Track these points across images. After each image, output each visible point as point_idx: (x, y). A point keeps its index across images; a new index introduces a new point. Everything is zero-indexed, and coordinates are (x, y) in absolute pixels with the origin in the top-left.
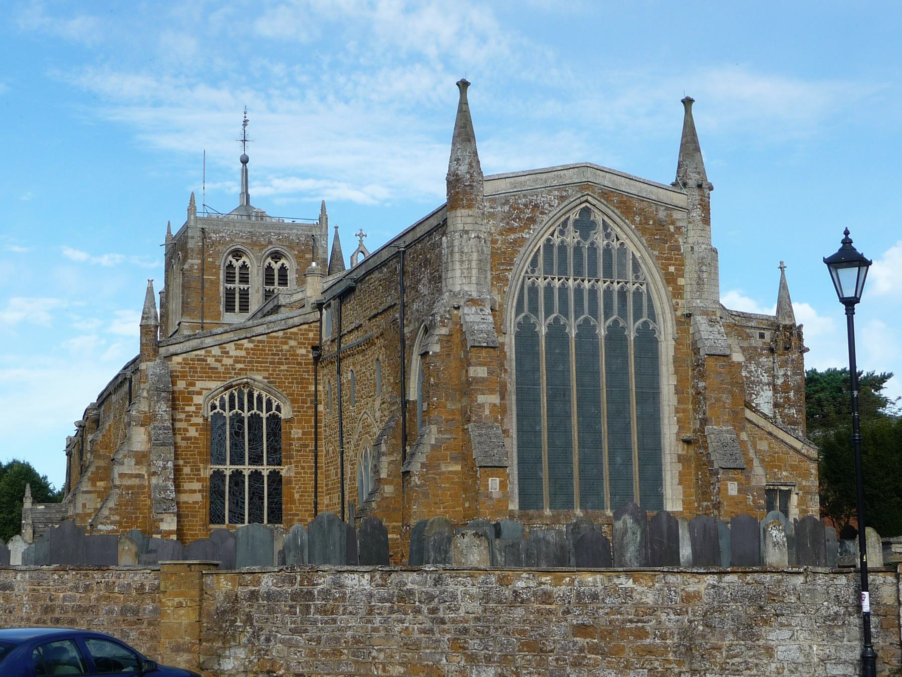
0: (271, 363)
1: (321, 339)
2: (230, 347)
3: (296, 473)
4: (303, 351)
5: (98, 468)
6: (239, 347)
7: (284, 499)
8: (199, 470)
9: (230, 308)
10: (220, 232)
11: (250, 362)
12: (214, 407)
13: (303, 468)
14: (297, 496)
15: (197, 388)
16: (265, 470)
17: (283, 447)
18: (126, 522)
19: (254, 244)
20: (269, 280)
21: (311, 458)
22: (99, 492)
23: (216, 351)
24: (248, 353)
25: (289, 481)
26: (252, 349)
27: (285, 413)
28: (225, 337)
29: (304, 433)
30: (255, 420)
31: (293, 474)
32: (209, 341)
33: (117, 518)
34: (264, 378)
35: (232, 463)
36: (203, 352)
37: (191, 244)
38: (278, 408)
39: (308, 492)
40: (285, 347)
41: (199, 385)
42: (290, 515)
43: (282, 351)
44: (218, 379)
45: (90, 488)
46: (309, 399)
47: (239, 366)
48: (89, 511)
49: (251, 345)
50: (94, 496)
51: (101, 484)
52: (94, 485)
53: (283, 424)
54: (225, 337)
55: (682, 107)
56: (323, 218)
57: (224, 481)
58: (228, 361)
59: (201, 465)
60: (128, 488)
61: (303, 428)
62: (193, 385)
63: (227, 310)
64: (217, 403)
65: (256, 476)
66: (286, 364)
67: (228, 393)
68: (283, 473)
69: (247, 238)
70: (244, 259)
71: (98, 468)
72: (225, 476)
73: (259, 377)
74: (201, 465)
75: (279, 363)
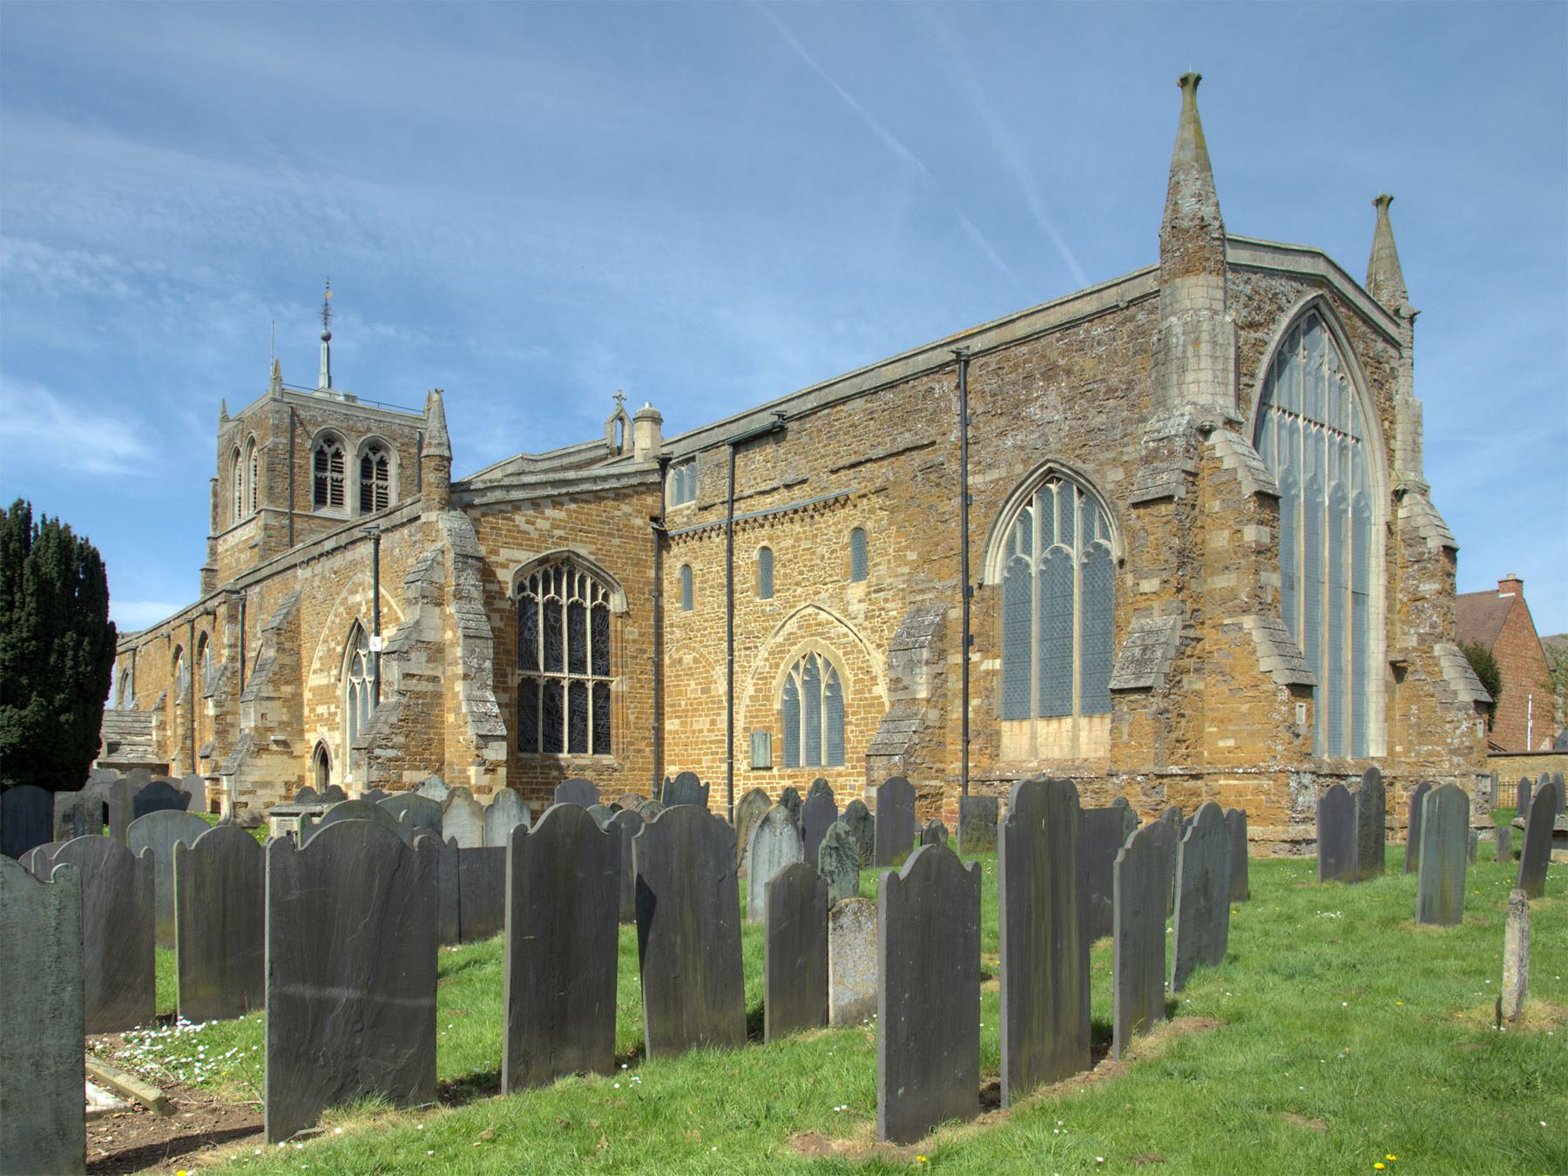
0: (601, 533)
4: (639, 522)
5: (282, 666)
7: (613, 721)
8: (505, 676)
11: (572, 529)
13: (640, 681)
15: (501, 559)
17: (612, 650)
22: (286, 700)
29: (642, 635)
33: (401, 739)
35: (561, 670)
38: (606, 597)
40: (617, 513)
41: (505, 554)
44: (531, 548)
47: (558, 532)
52: (277, 688)
53: (612, 619)
55: (1372, 213)
57: (536, 695)
58: (543, 524)
59: (509, 670)
62: (496, 553)
64: (527, 583)
67: (541, 569)
72: (537, 686)
73: (583, 552)
74: (509, 670)
75: (612, 535)
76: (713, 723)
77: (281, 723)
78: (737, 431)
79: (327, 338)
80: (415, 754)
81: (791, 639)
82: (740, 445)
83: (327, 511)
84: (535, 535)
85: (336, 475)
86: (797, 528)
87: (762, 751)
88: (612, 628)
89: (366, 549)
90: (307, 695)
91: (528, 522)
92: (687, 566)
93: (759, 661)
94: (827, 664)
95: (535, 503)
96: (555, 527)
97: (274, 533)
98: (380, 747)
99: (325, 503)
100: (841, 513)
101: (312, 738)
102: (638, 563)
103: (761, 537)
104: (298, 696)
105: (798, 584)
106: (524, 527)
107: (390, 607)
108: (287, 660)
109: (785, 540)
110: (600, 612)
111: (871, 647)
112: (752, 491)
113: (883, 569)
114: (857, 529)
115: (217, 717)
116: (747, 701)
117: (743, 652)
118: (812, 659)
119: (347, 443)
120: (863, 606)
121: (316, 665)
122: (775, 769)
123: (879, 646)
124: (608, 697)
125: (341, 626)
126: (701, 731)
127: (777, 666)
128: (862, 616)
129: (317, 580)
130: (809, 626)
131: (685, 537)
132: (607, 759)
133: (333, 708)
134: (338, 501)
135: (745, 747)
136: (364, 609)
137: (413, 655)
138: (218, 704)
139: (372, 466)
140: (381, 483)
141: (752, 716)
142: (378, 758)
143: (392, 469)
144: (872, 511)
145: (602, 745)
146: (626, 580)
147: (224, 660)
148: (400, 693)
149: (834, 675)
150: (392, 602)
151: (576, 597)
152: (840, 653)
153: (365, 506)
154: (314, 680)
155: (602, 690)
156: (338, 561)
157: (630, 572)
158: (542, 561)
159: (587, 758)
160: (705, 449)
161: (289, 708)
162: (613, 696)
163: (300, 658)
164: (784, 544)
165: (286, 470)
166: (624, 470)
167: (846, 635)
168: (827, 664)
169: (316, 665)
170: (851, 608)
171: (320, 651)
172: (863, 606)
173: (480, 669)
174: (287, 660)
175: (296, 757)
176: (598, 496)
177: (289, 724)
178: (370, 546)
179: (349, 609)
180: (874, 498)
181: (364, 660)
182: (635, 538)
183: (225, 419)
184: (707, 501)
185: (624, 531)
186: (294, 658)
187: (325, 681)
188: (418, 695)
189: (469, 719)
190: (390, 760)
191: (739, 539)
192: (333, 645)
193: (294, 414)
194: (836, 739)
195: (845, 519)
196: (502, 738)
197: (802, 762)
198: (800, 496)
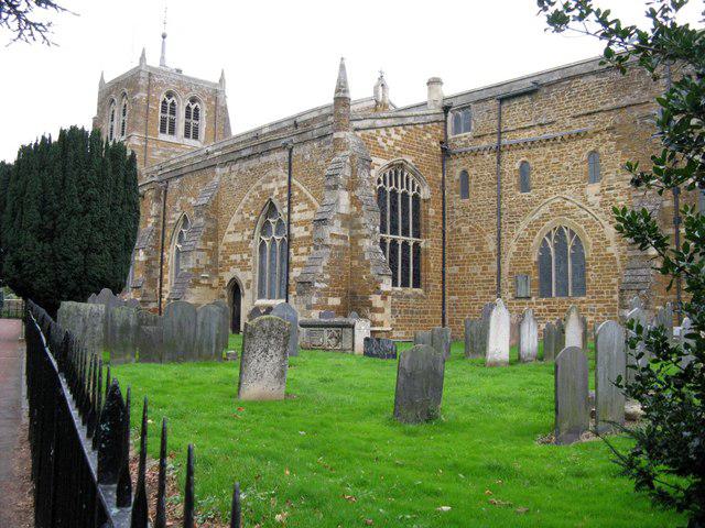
1: (447, 136)
2: (392, 131)
6: (397, 132)
9: (163, 130)
12: (379, 182)
14: (432, 265)
16: (411, 240)
20: (188, 115)
21: (440, 234)
23: (383, 132)
27: (425, 193)
28: (390, 122)
30: (405, 195)
32: (379, 123)
33: (328, 276)
36: (374, 131)
37: (142, 82)
38: (418, 190)
44: (384, 157)
47: (398, 148)
49: (404, 132)
51: (210, 243)
54: (390, 122)
56: (222, 80)
60: (337, 248)
63: (161, 132)
65: (405, 244)
68: (422, 245)
70: (173, 98)
73: (409, 161)
76: (485, 269)
77: (207, 266)
78: (501, 92)
81: (545, 218)
82: (502, 100)
84: (386, 149)
86: (548, 150)
87: (523, 287)
89: (282, 156)
90: (222, 248)
92: (465, 172)
93: (521, 230)
94: (572, 233)
96: (396, 144)
99: (165, 132)
100: (580, 143)
103: (522, 155)
105: (548, 184)
107: (301, 192)
109: (538, 158)
110: (416, 198)
111: (605, 223)
112: (514, 128)
113: (612, 176)
114: (594, 152)
116: (512, 256)
117: (508, 225)
118: (560, 230)
120: (599, 198)
122: (533, 299)
123: (611, 223)
126: (476, 274)
127: (534, 234)
128: (598, 204)
129: (233, 176)
130: (558, 210)
131: (464, 154)
135: (509, 284)
136: (276, 193)
138: (147, 254)
139: (193, 114)
141: (514, 264)
143: (203, 114)
144: (604, 141)
149: (577, 239)
151: (405, 189)
152: (582, 226)
153: (187, 135)
158: (391, 166)
160: (476, 102)
164: (538, 160)
166: (418, 113)
167: (586, 216)
168: (572, 233)
169: (231, 228)
170: (589, 200)
171: (236, 218)
172: (599, 198)
178: (285, 154)
180: (605, 134)
184: (479, 133)
187: (240, 239)
191: (505, 155)
194: (578, 280)
195: (584, 146)
197: (554, 294)
198: (549, 132)
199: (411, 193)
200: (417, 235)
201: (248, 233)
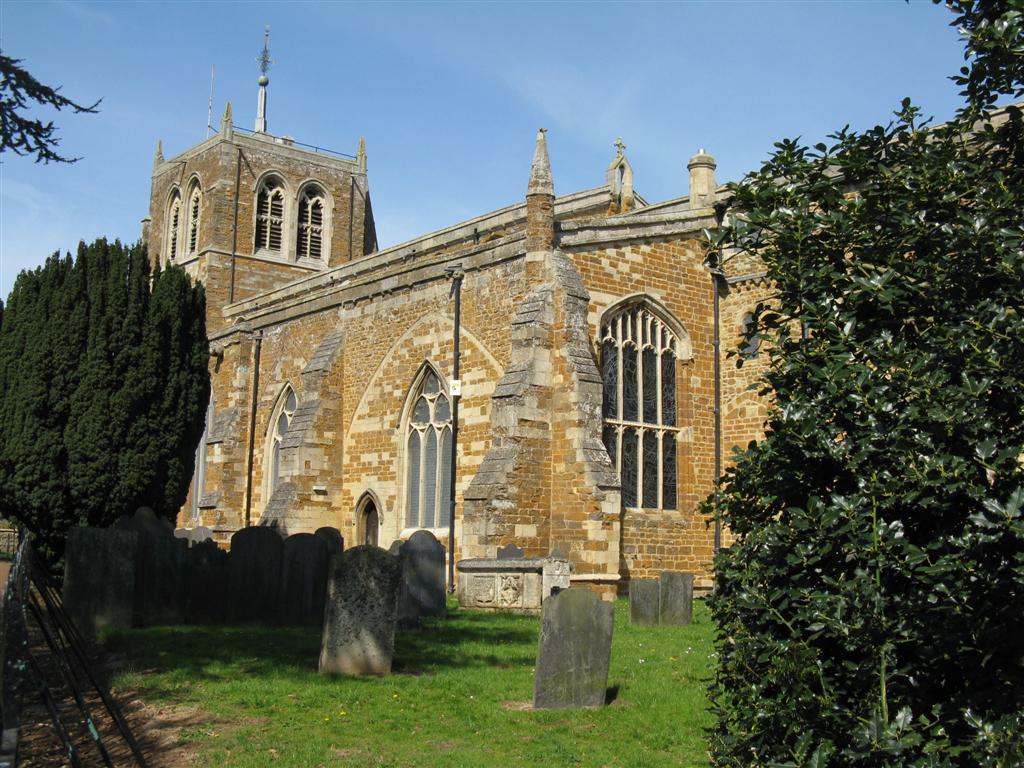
0: (670, 278)
3: (696, 439)
5: (326, 411)
10: (256, 153)
11: (647, 273)
13: (702, 432)
14: (696, 471)
18: (527, 498)
19: (291, 173)
21: (711, 419)
22: (328, 447)
24: (645, 260)
25: (687, 448)
26: (650, 255)
29: (704, 383)
31: (691, 440)
34: (662, 298)
35: (636, 420)
39: (707, 466)
40: (684, 258)
42: (689, 497)
43: (679, 263)
44: (613, 292)
45: (316, 441)
46: (708, 335)
47: (636, 276)
48: (313, 474)
50: (319, 451)
51: (328, 435)
52: (320, 436)
58: (624, 268)
61: (702, 375)
66: (685, 283)
68: (679, 437)
69: (284, 165)
71: (326, 411)
73: (657, 297)
75: (678, 280)
77: (323, 472)
79: (264, 84)
80: (526, 506)
83: (265, 254)
84: (617, 278)
85: (275, 218)
88: (677, 376)
90: (348, 442)
91: (612, 265)
95: (617, 244)
96: (633, 270)
97: (216, 274)
98: (497, 498)
101: (356, 491)
102: (701, 310)
104: (338, 442)
106: (609, 269)
107: (475, 350)
108: (330, 404)
115: (225, 464)
119: (286, 184)
121: (363, 409)
124: (674, 449)
125: (402, 369)
129: (368, 323)
132: (675, 515)
133: (386, 456)
134: (276, 244)
136: (436, 351)
137: (527, 399)
140: (315, 227)
142: (495, 509)
143: (327, 214)
145: (670, 503)
146: (690, 326)
147: (232, 404)
148: (516, 440)
150: (478, 344)
151: (649, 343)
153: (300, 250)
154: (358, 425)
155: (669, 437)
156: (401, 301)
157: (694, 318)
159: (659, 513)
161: (330, 455)
162: (678, 448)
163: (341, 403)
165: (232, 211)
171: (371, 393)
173: (593, 416)
174: (330, 404)
175: (333, 509)
176: (666, 238)
177: (329, 473)
179: (414, 353)
181: (432, 406)
182: (698, 284)
183: (161, 160)
185: (688, 276)
186: (337, 402)
187: (377, 427)
188: (530, 442)
189: (587, 468)
190: (505, 512)
192: (388, 389)
193: (241, 155)
196: (617, 488)
199: (659, 351)
200: (669, 419)
201: (389, 418)
